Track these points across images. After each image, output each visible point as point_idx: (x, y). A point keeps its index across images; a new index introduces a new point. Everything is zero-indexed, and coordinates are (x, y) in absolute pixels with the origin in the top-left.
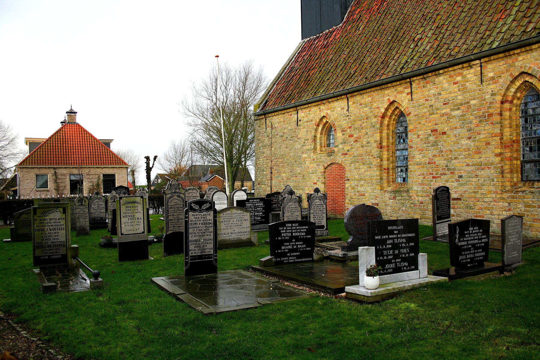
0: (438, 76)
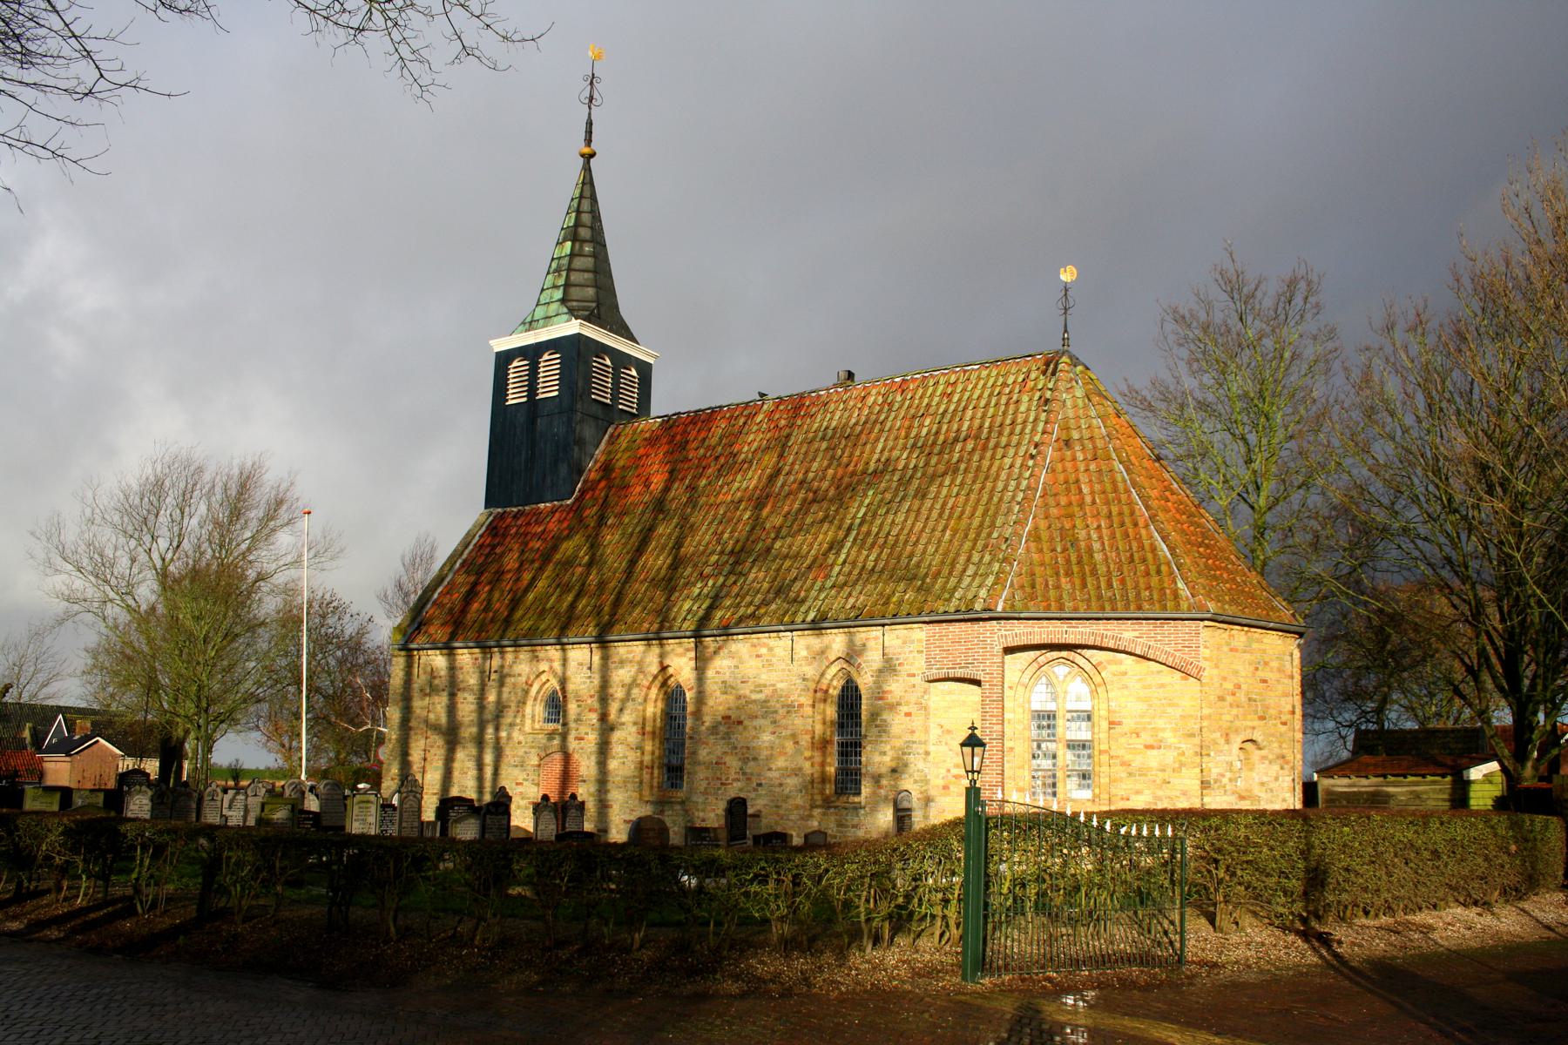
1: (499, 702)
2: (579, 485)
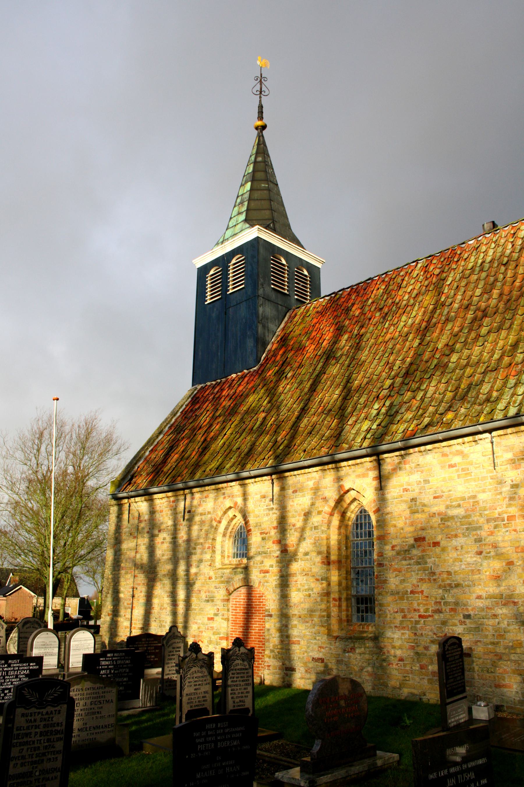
0: (424, 453)
1: (189, 541)
2: (264, 355)
